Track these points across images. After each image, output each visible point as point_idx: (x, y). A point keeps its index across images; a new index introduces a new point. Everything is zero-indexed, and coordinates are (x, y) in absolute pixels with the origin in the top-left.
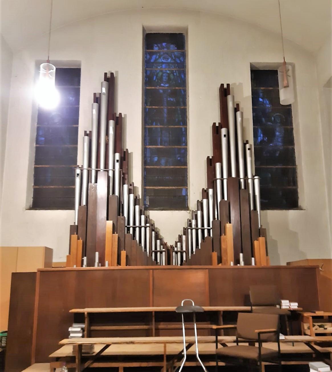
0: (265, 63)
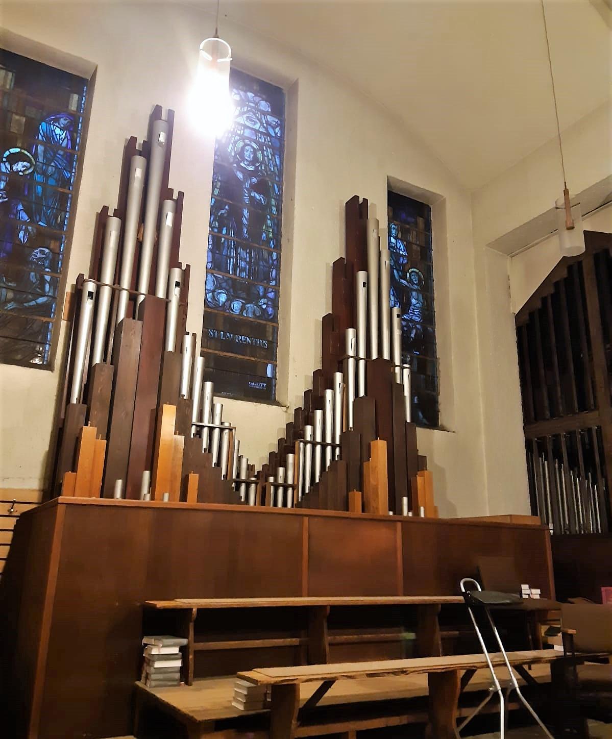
0: (405, 182)
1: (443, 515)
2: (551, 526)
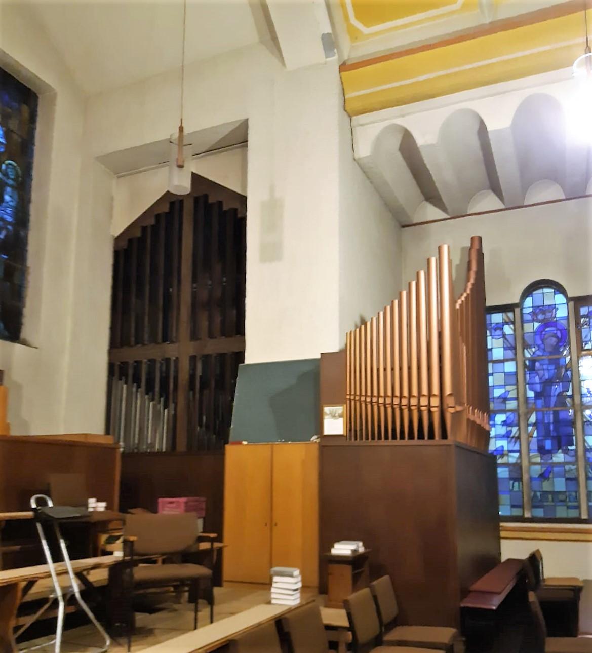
1: (15, 432)
2: (121, 444)
